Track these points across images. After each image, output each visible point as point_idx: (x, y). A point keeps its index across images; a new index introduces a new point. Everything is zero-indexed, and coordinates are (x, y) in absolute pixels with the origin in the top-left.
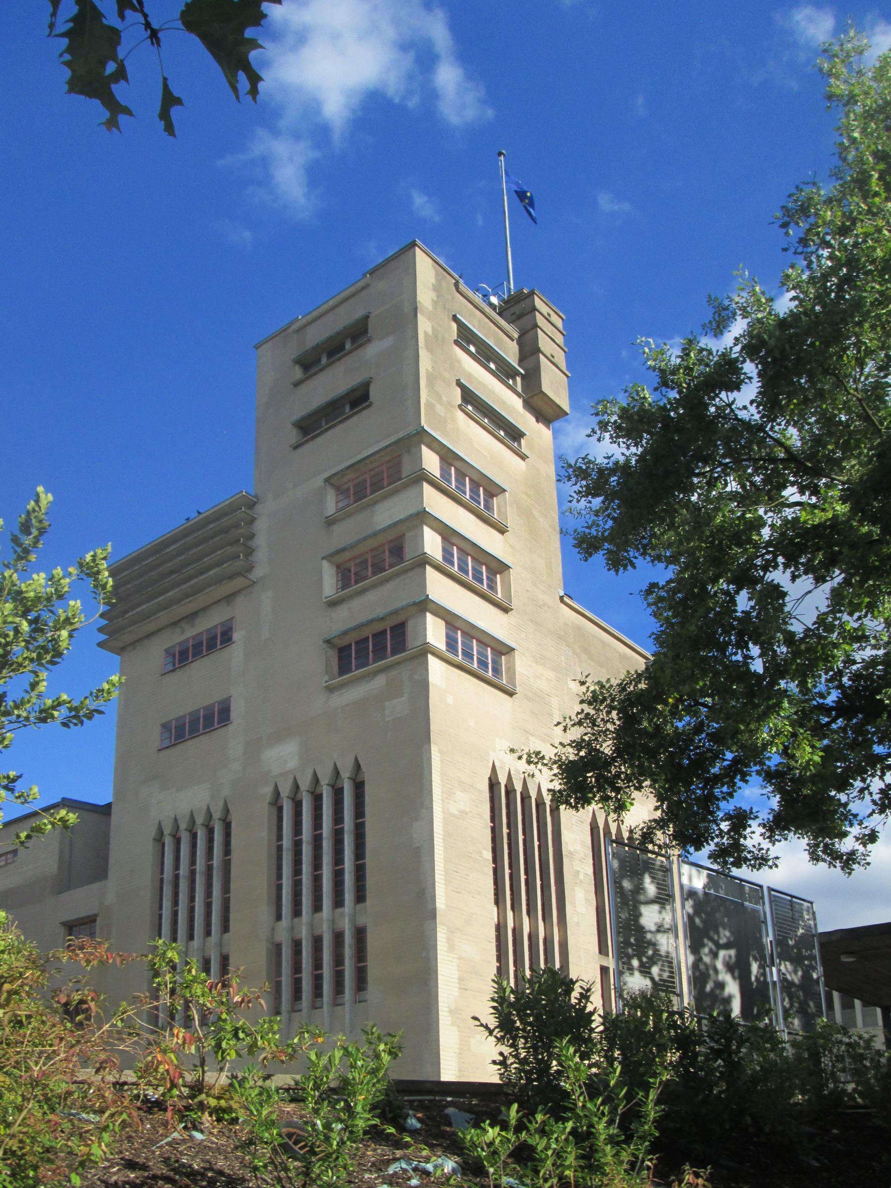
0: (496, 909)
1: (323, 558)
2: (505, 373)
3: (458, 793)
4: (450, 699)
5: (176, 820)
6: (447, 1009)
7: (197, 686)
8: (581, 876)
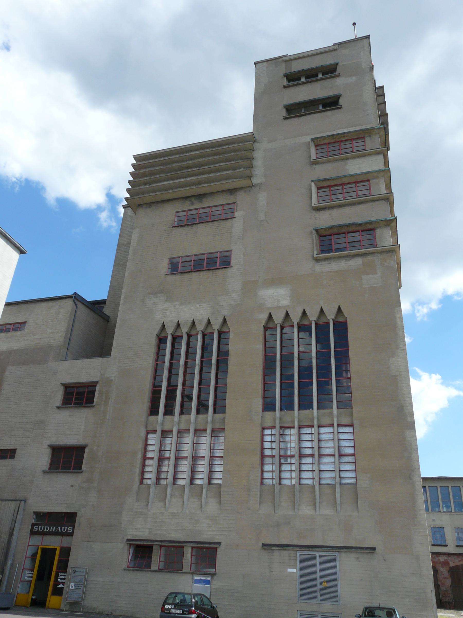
1: (312, 181)
5: (193, 323)
7: (201, 240)
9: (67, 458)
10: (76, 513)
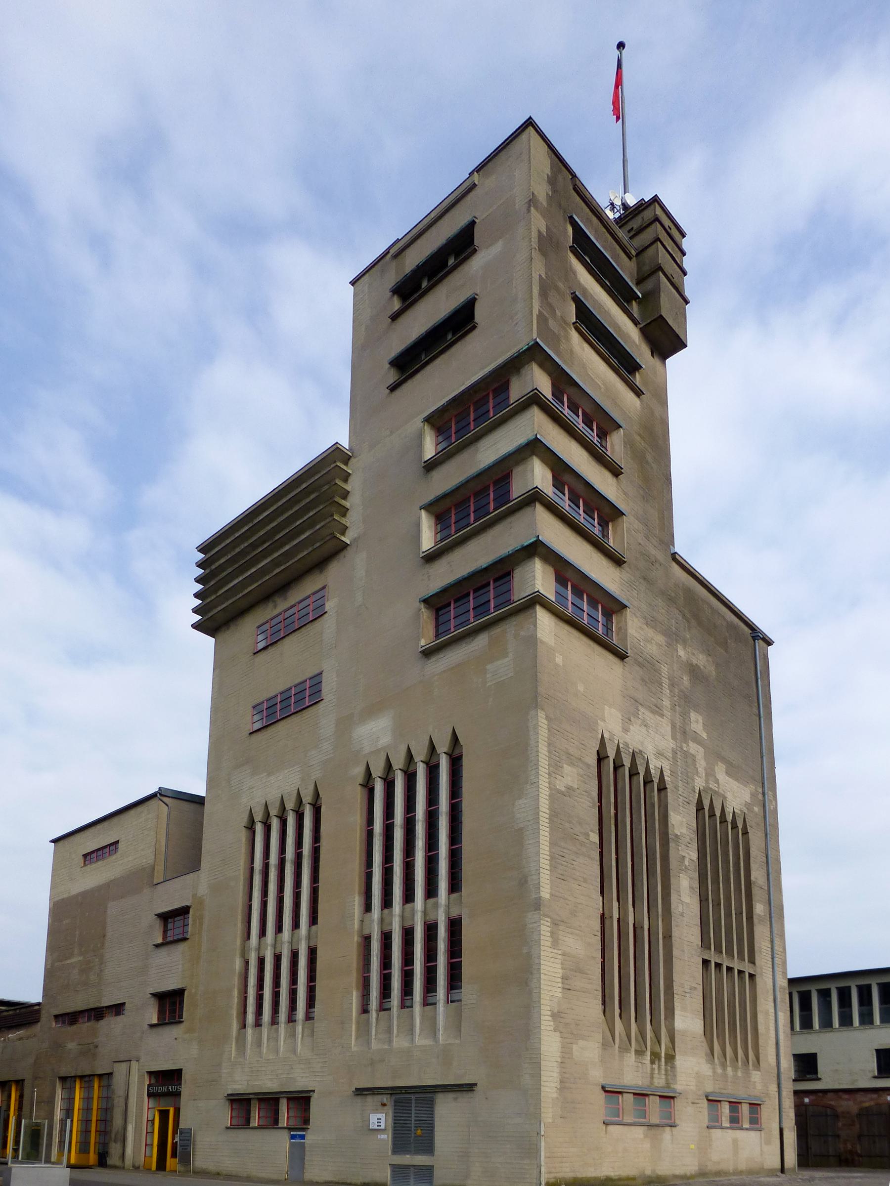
0: (601, 898)
2: (621, 293)
3: (565, 766)
4: (559, 660)
6: (549, 1013)
8: (687, 863)
9: (171, 1004)
10: (181, 1070)
